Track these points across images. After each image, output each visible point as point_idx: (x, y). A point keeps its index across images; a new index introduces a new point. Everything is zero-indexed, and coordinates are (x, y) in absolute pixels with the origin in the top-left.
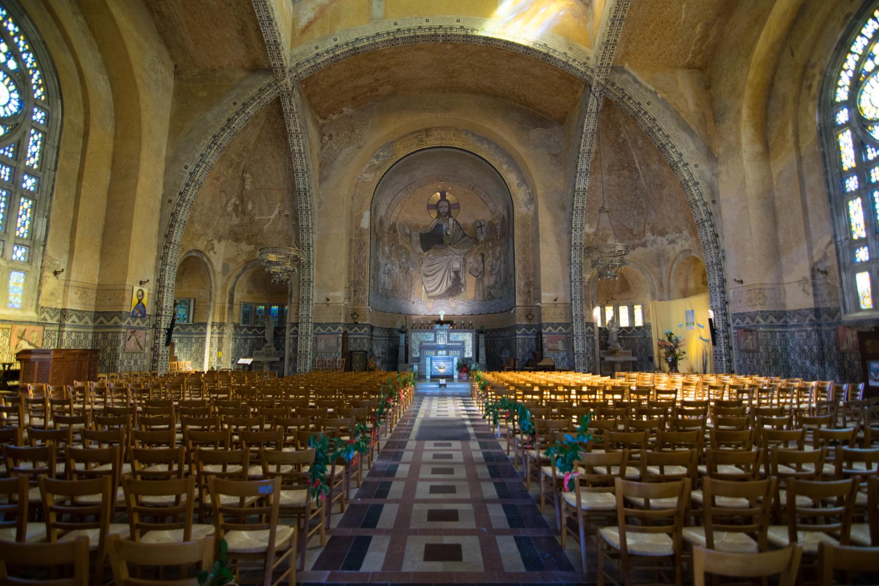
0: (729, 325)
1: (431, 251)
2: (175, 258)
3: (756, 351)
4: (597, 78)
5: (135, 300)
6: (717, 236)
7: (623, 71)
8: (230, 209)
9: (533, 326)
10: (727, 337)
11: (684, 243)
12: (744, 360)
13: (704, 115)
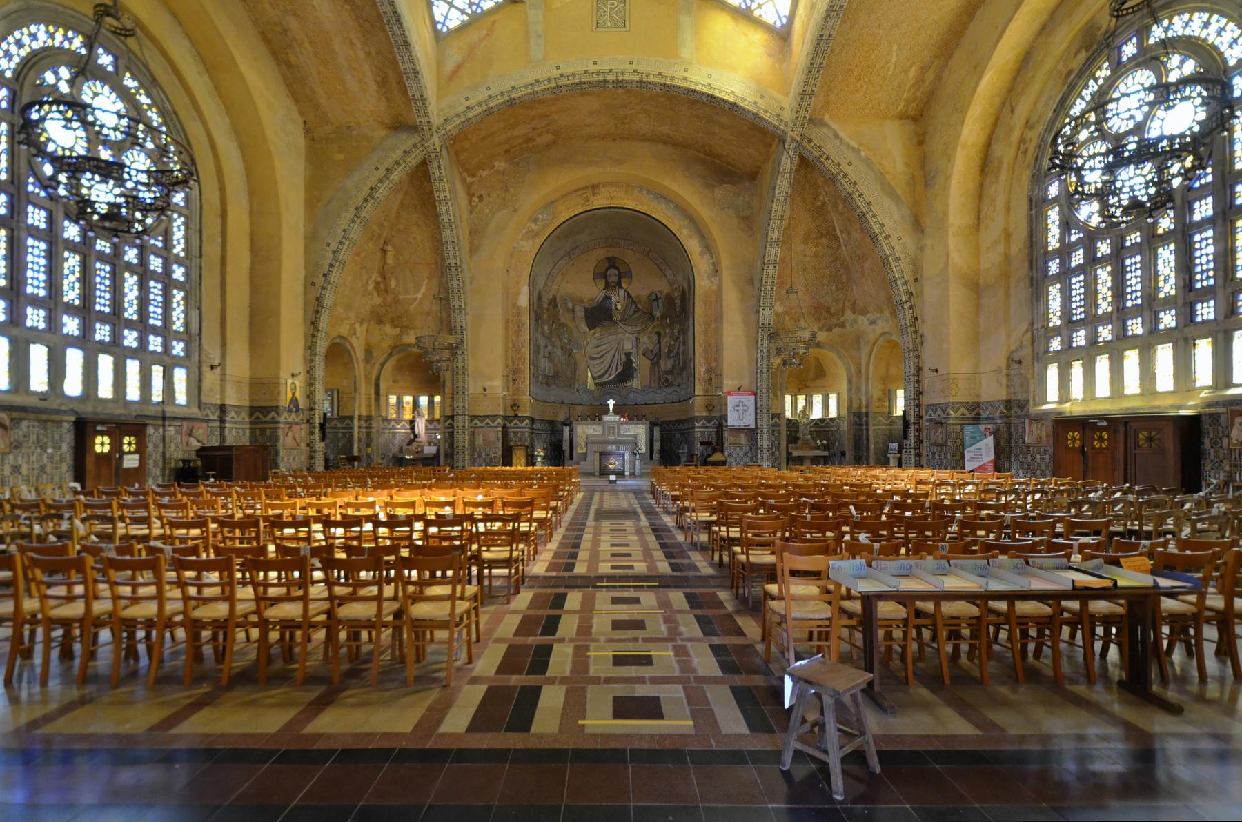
0: (921, 417)
1: (598, 329)
2: (322, 346)
3: (944, 445)
4: (792, 133)
5: (290, 395)
6: (916, 319)
7: (822, 123)
8: (371, 286)
9: (714, 418)
10: (918, 430)
11: (884, 325)
12: (933, 454)
13: (913, 177)
